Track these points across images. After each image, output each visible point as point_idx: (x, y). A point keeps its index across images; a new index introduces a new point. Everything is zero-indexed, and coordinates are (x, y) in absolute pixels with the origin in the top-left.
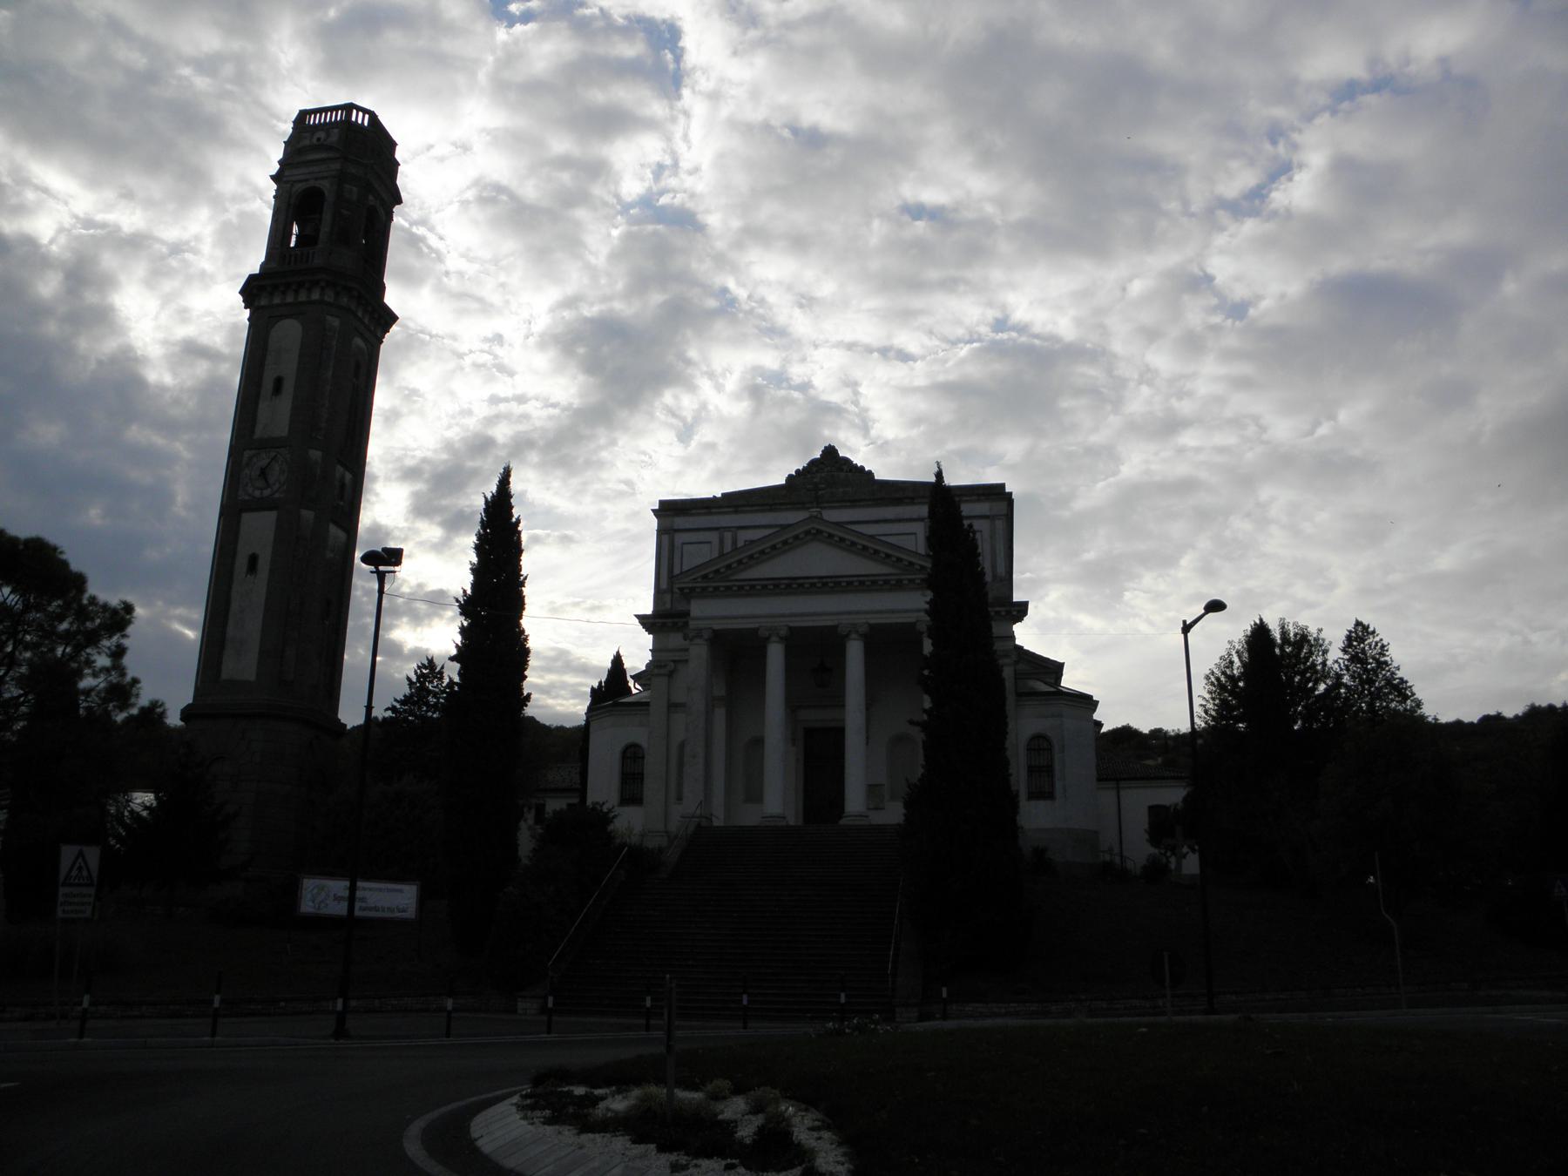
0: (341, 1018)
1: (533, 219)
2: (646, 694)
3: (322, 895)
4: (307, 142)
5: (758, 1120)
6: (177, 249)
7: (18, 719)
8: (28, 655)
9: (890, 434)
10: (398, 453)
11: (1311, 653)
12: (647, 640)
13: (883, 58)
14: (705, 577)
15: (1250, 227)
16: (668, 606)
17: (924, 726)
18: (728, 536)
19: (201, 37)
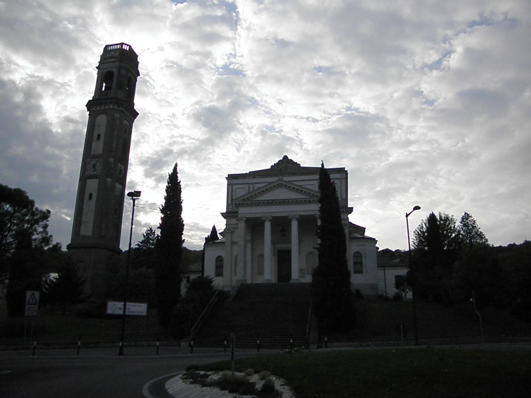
0: (121, 348)
1: (186, 73)
2: (224, 239)
3: (114, 307)
4: (108, 56)
5: (263, 382)
6: (63, 85)
7: (11, 249)
8: (15, 227)
9: (309, 148)
10: (139, 156)
11: (450, 224)
12: (224, 221)
13: (308, 15)
14: (244, 200)
15: (435, 73)
16: (231, 209)
17: (318, 249)
18: (251, 186)
19: (70, 10)
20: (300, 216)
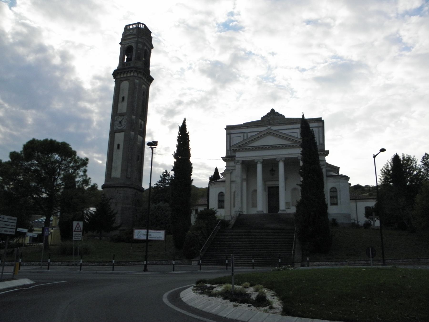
14: (240, 146)
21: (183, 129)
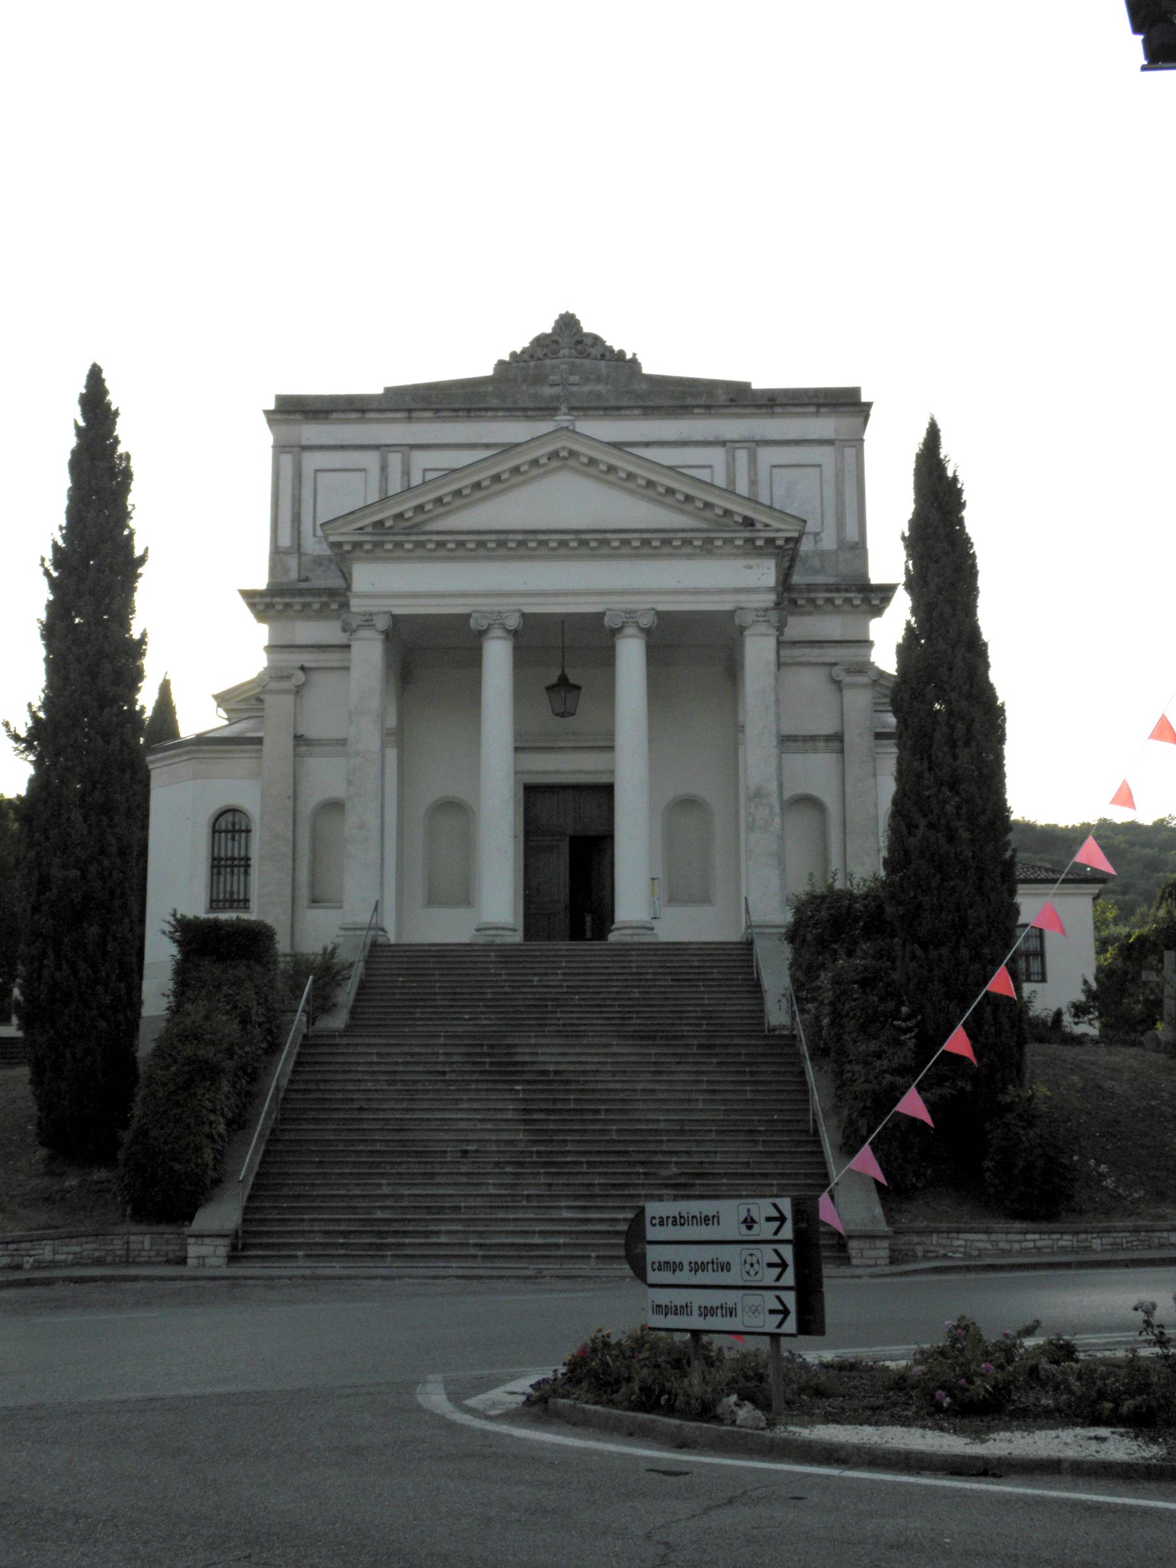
12: (261, 633)
20: (660, 615)
21: (96, 405)
